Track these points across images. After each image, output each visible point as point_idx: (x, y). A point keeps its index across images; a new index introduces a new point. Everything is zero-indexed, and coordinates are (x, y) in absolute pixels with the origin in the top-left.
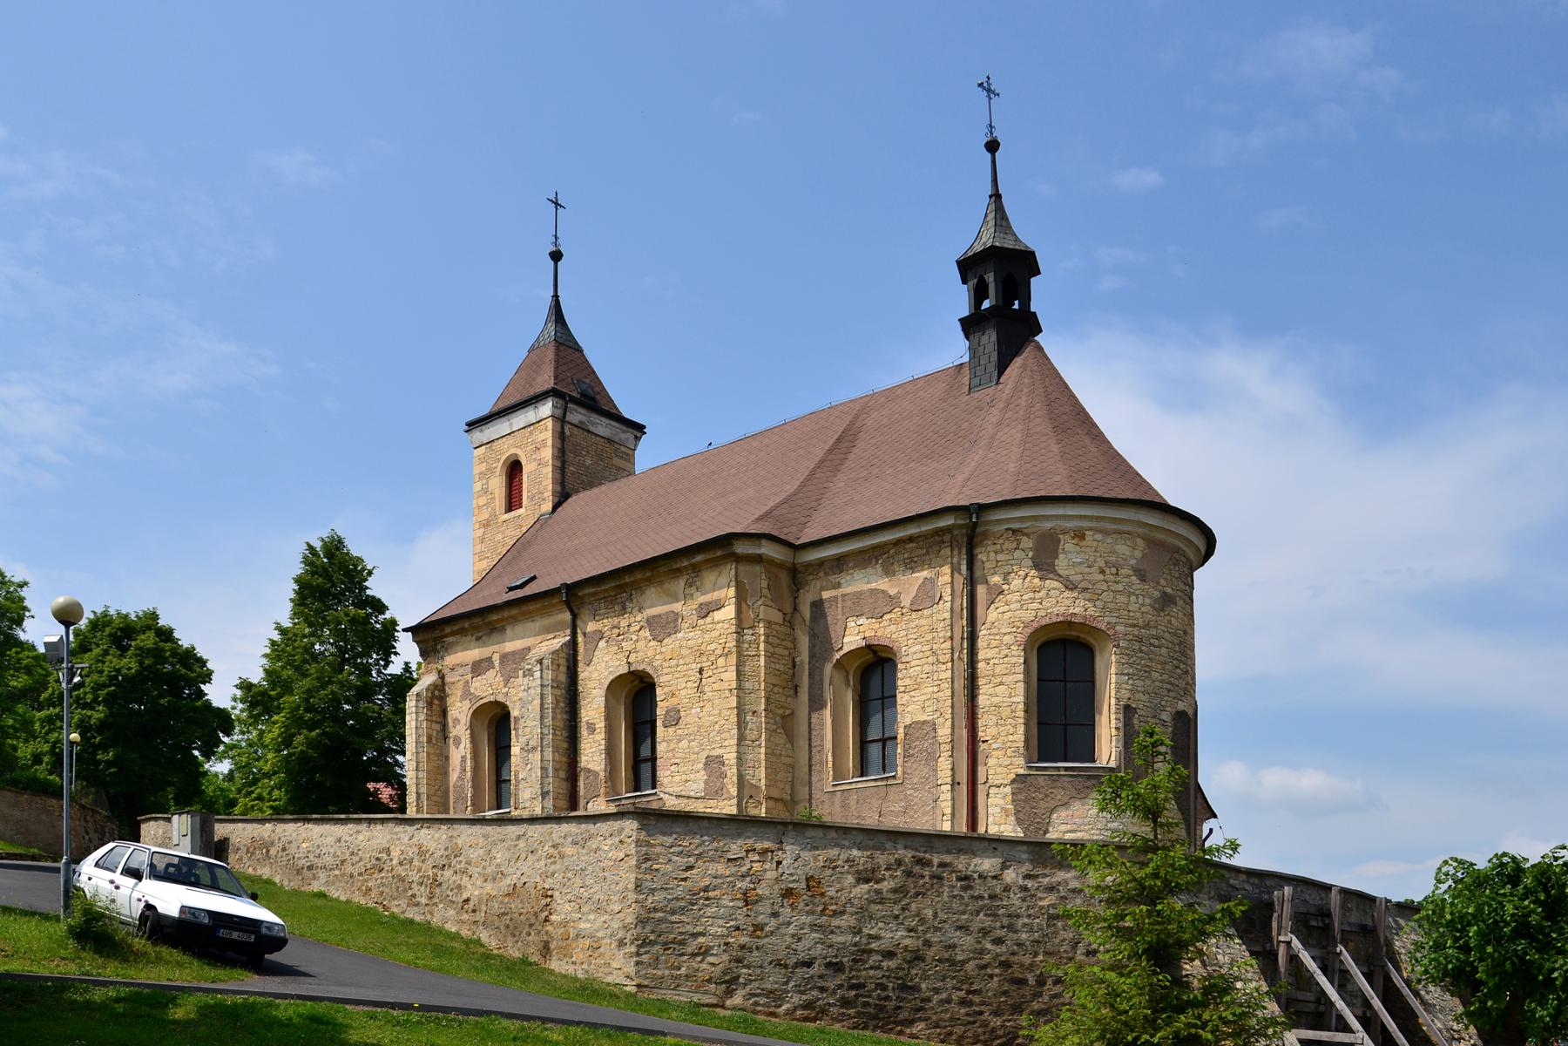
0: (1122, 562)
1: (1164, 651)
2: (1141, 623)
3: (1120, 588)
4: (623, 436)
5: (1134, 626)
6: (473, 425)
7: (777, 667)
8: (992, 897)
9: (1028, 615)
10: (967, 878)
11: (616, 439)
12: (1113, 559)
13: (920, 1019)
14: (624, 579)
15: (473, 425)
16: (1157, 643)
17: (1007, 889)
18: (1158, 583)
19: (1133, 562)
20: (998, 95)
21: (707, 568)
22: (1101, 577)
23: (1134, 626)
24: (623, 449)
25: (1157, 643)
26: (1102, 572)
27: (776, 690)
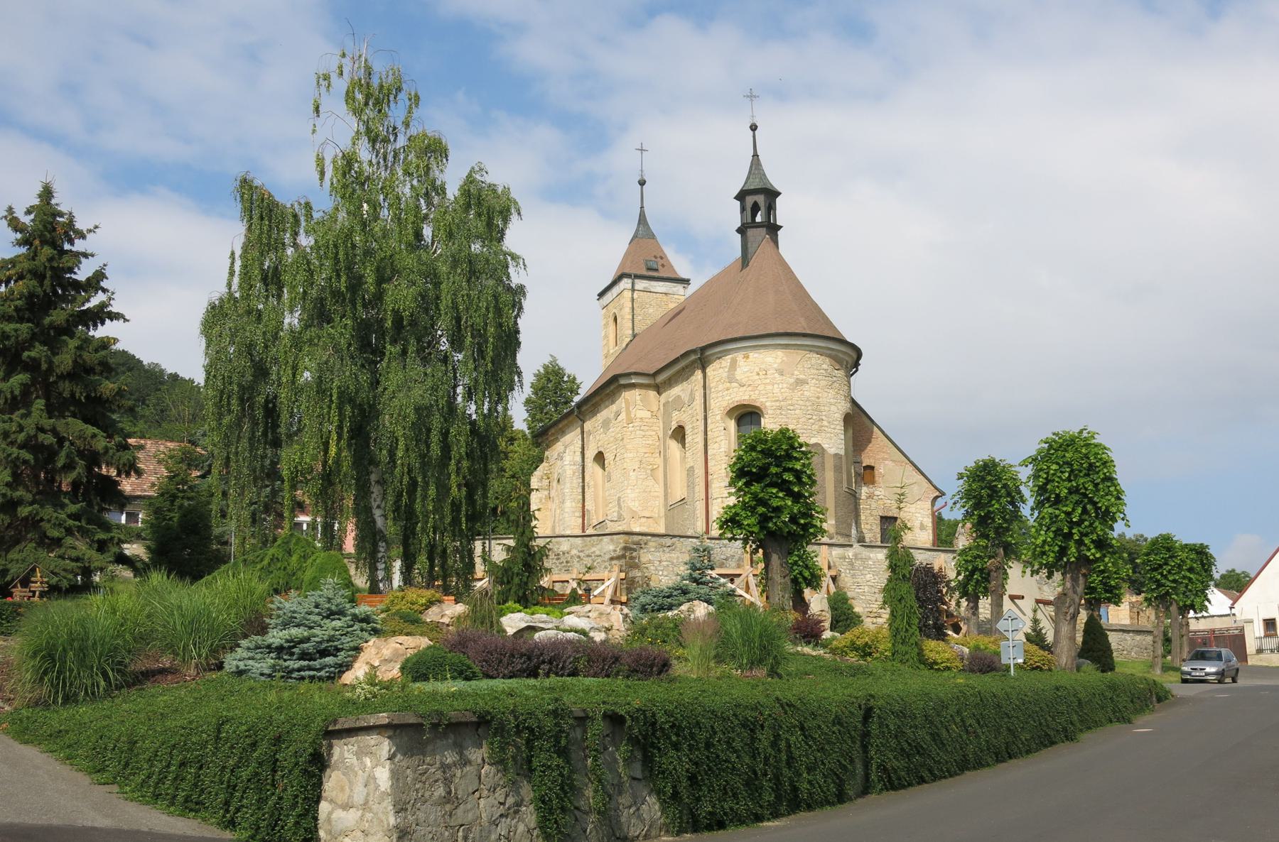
0: (769, 367)
1: (797, 412)
2: (781, 399)
3: (768, 381)
4: (675, 289)
5: (775, 401)
6: (601, 295)
7: (647, 442)
8: (567, 562)
9: (725, 404)
10: (558, 555)
11: (670, 292)
12: (763, 366)
13: (30, 680)
14: (189, 505)
15: (601, 295)
16: (792, 408)
17: (572, 557)
18: (793, 374)
19: (775, 366)
20: (105, 265)
21: (601, 400)
22: (758, 377)
23: (775, 401)
24: (676, 296)
25: (792, 408)
26: (758, 374)
27: (646, 455)
